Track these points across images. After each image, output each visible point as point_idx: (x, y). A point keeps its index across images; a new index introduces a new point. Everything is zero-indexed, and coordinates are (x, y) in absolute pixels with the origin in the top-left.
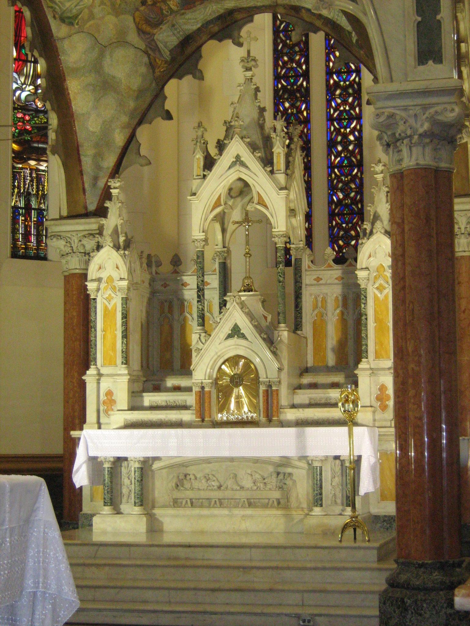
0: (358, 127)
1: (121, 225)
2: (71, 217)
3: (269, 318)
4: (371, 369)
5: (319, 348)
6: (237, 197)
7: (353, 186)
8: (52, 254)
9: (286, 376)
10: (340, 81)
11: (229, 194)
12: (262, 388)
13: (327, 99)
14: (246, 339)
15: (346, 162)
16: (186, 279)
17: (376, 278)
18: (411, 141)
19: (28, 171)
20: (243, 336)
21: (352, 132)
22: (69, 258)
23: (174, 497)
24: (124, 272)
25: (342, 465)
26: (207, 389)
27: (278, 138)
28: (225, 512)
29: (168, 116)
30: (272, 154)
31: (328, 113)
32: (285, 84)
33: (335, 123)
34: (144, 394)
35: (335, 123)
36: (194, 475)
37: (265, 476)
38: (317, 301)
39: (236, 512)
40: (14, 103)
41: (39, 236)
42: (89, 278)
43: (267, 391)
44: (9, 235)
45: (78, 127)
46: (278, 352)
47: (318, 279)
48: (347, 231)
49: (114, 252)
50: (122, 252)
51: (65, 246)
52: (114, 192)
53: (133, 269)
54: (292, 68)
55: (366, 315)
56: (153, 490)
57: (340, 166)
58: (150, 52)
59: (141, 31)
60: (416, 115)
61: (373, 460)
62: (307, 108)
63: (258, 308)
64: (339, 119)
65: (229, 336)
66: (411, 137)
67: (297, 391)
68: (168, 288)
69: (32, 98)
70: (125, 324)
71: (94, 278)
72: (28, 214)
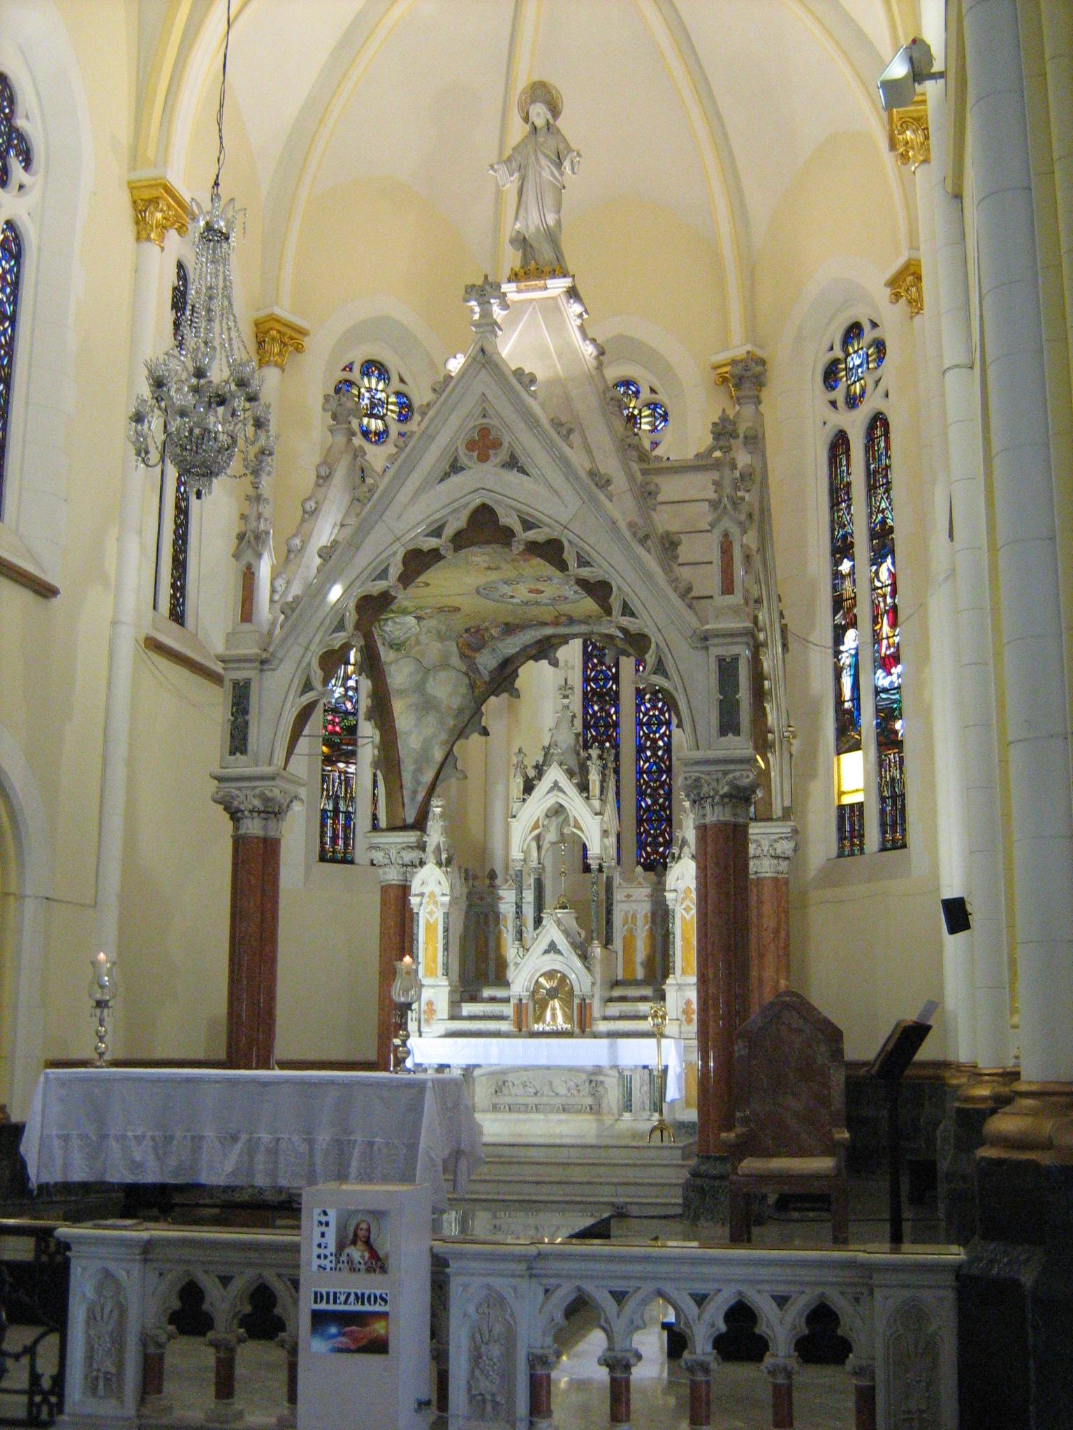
2: (392, 828)
3: (583, 935)
5: (628, 962)
7: (662, 792)
12: (577, 1001)
14: (562, 954)
17: (683, 899)
19: (337, 774)
20: (559, 952)
21: (661, 738)
22: (387, 869)
26: (524, 1001)
28: (541, 1116)
30: (588, 780)
31: (637, 718)
38: (627, 918)
39: (552, 1117)
40: (325, 705)
41: (346, 839)
47: (629, 896)
48: (655, 837)
49: (437, 869)
54: (602, 671)
57: (649, 772)
58: (471, 674)
59: (463, 656)
61: (678, 1070)
62: (616, 712)
63: (572, 923)
64: (649, 724)
65: (546, 952)
66: (713, 797)
67: (609, 1004)
69: (342, 700)
70: (446, 937)
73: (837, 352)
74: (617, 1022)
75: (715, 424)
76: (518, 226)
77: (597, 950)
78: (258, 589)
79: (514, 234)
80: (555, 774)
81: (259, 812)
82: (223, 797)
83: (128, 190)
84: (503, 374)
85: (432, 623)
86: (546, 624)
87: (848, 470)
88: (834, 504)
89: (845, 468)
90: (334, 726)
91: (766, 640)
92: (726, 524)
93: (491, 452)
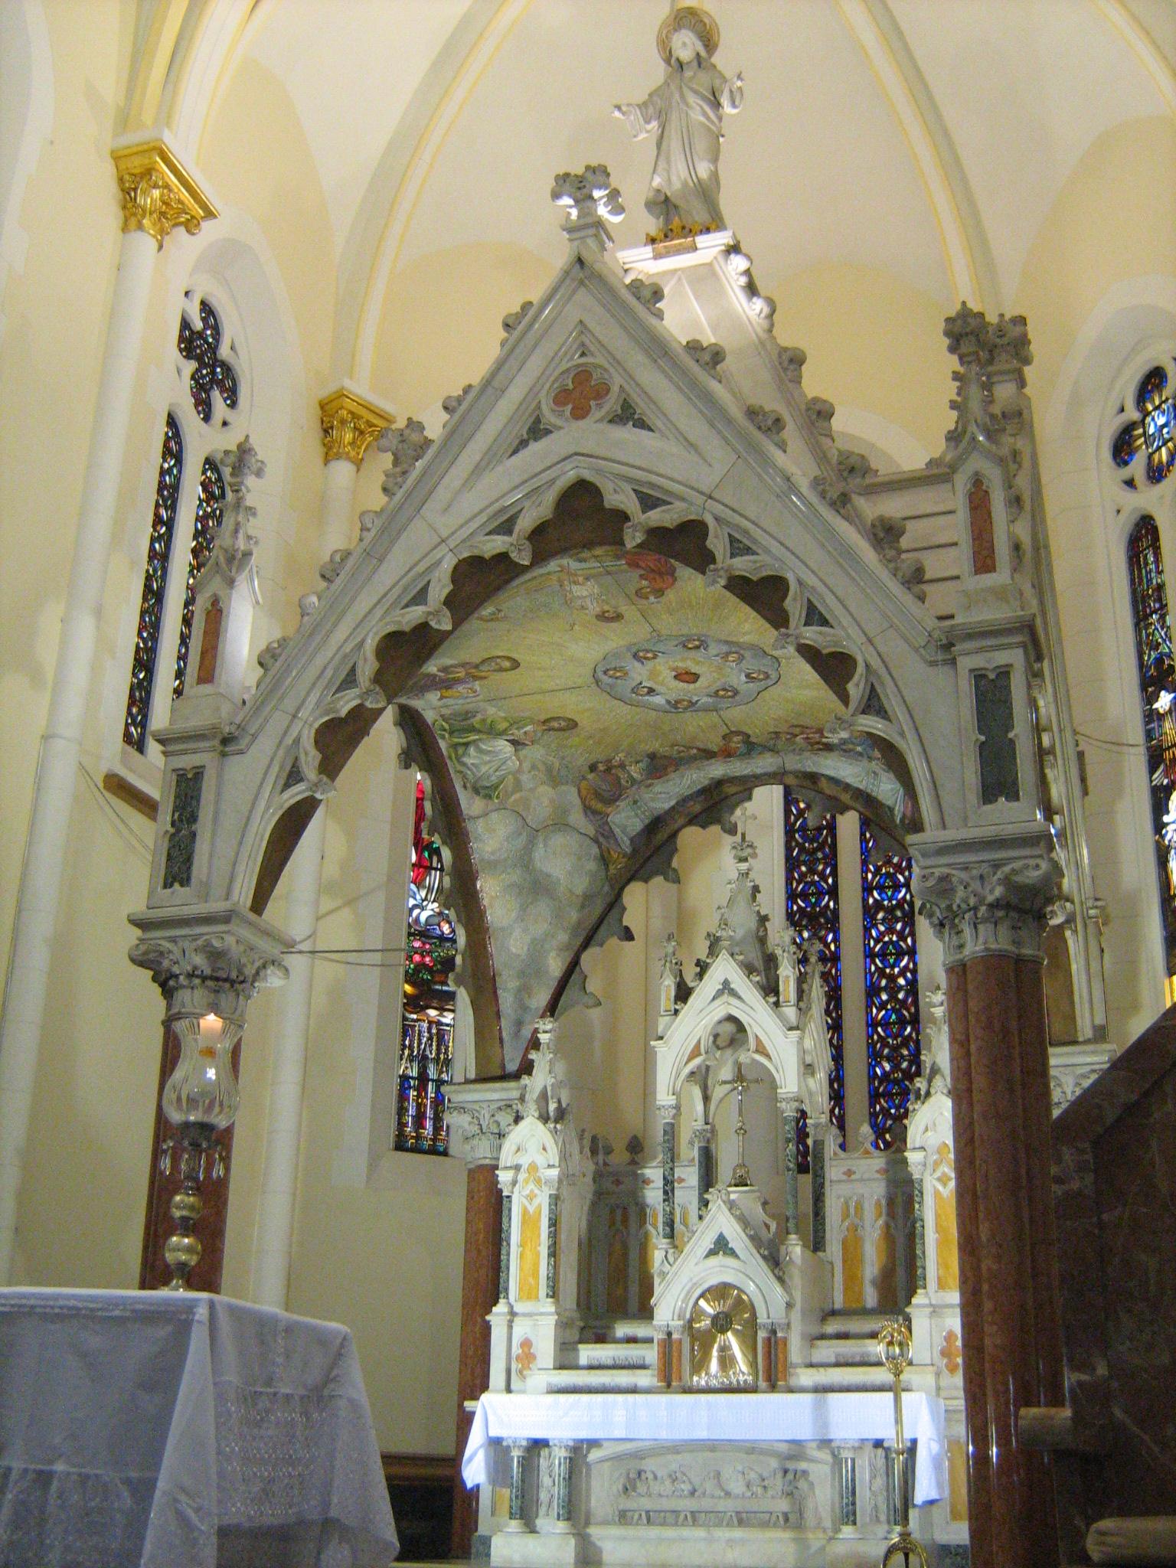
0: (911, 966)
1: (552, 1085)
2: (482, 1079)
3: (773, 1227)
4: (931, 1305)
5: (852, 1279)
6: (726, 1047)
7: (905, 1052)
8: (455, 1146)
9: (799, 1315)
10: (883, 900)
11: (714, 1042)
12: (762, 1335)
13: (864, 926)
14: (737, 1257)
15: (894, 1017)
16: (648, 1172)
18: (975, 914)
19: (425, 1025)
20: (732, 1253)
21: (902, 973)
22: (475, 1142)
23: (621, 1507)
24: (553, 1156)
25: (887, 1457)
26: (675, 1336)
27: (785, 955)
28: (700, 1533)
29: (628, 935)
31: (866, 945)
32: (803, 905)
33: (877, 961)
34: (580, 1346)
35: (877, 961)
36: (653, 1473)
37: (765, 1474)
38: (848, 1207)
42: (502, 1164)
43: (769, 1339)
44: (394, 1119)
45: (492, 948)
46: (786, 1278)
49: (540, 1125)
50: (552, 1126)
51: (470, 1123)
52: (544, 1038)
53: (567, 1155)
54: (813, 883)
55: (922, 1220)
56: (588, 1496)
57: (885, 1023)
58: (601, 839)
59: (587, 809)
60: (981, 877)
61: (935, 1447)
62: (836, 940)
63: (758, 1213)
64: (883, 955)
65: (712, 1253)
66: (975, 909)
67: (819, 1343)
68: (622, 1187)
69: (436, 920)
70: (554, 1235)
71: (509, 1165)
72: (422, 1087)
73: (1134, 415)
74: (831, 1370)
75: (948, 320)
76: (657, 181)
77: (795, 1249)
78: (226, 631)
79: (651, 194)
80: (724, 969)
81: (204, 978)
82: (145, 953)
83: (113, 162)
84: (611, 291)
85: (535, 753)
86: (708, 755)
87: (1157, 567)
88: (1141, 619)
89: (1153, 567)
90: (423, 957)
91: (1053, 746)
92: (977, 463)
93: (592, 403)
